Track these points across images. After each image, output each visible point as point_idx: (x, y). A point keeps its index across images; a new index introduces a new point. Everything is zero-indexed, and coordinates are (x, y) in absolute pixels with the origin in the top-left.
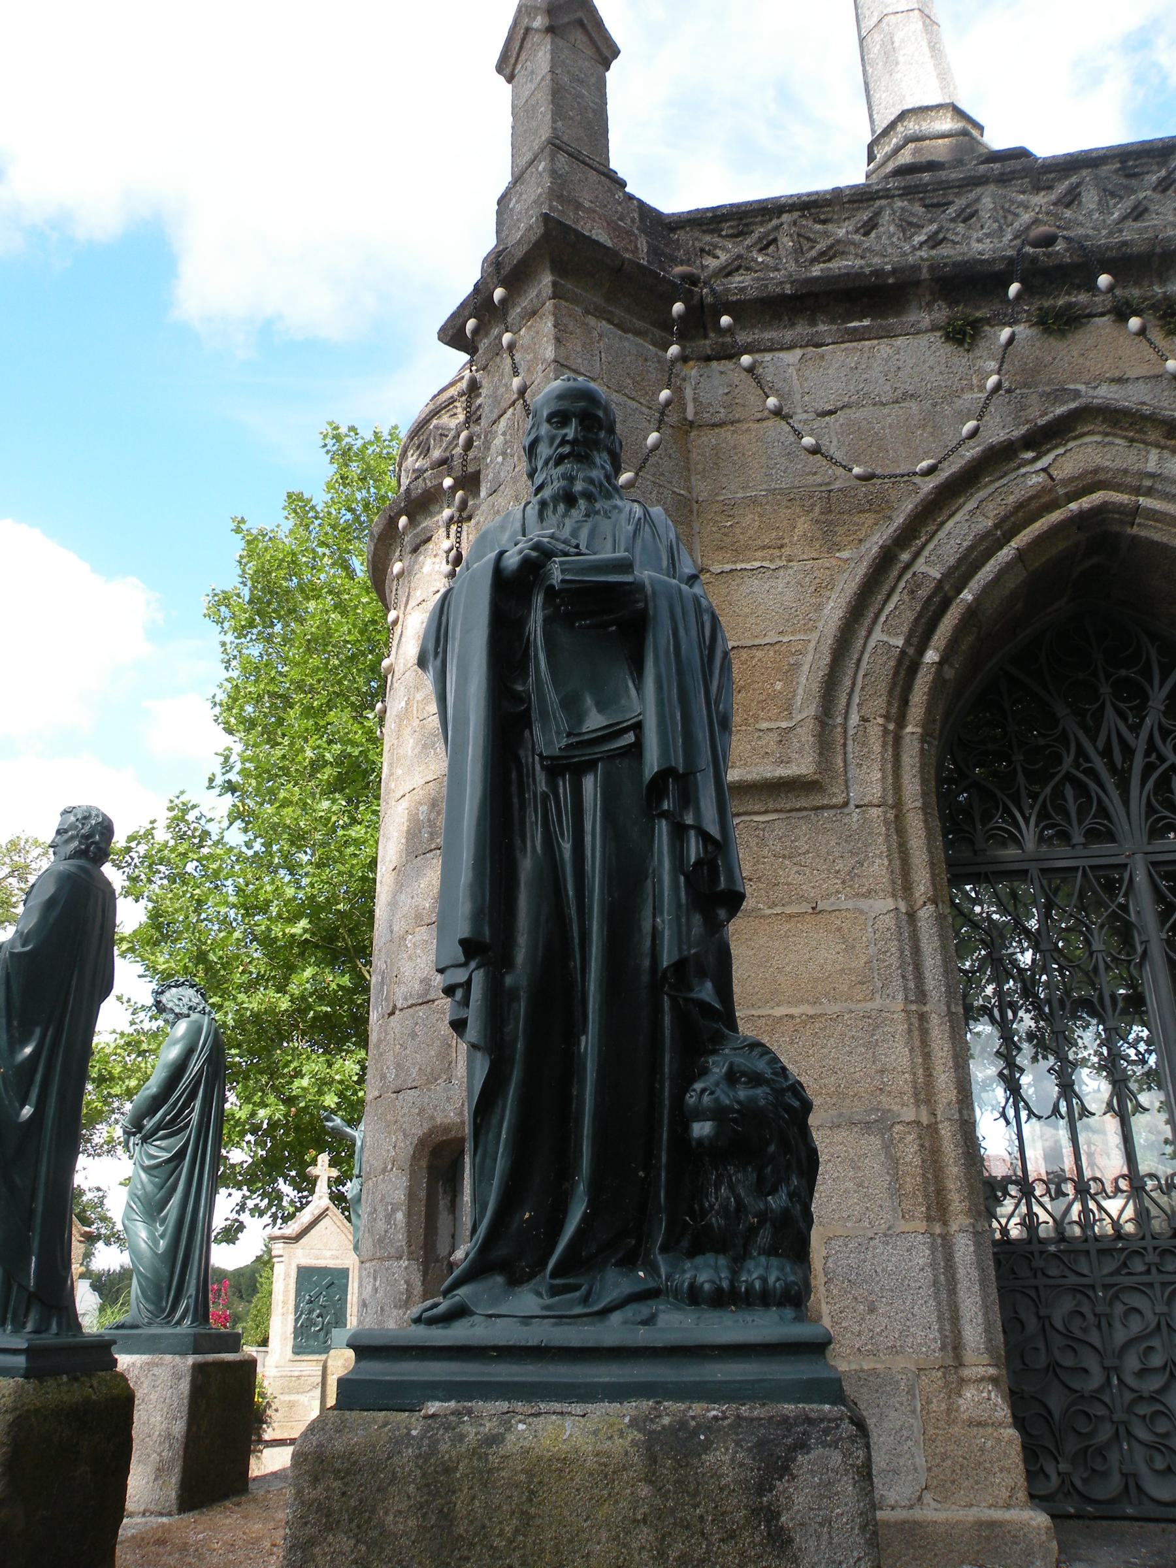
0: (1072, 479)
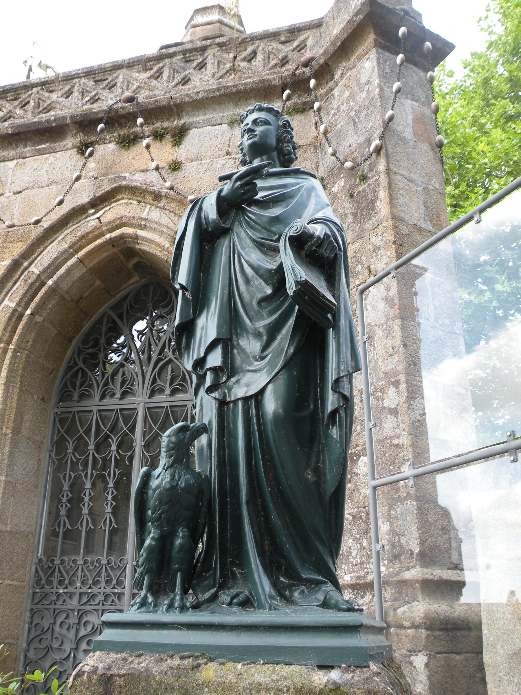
0: (110, 222)
